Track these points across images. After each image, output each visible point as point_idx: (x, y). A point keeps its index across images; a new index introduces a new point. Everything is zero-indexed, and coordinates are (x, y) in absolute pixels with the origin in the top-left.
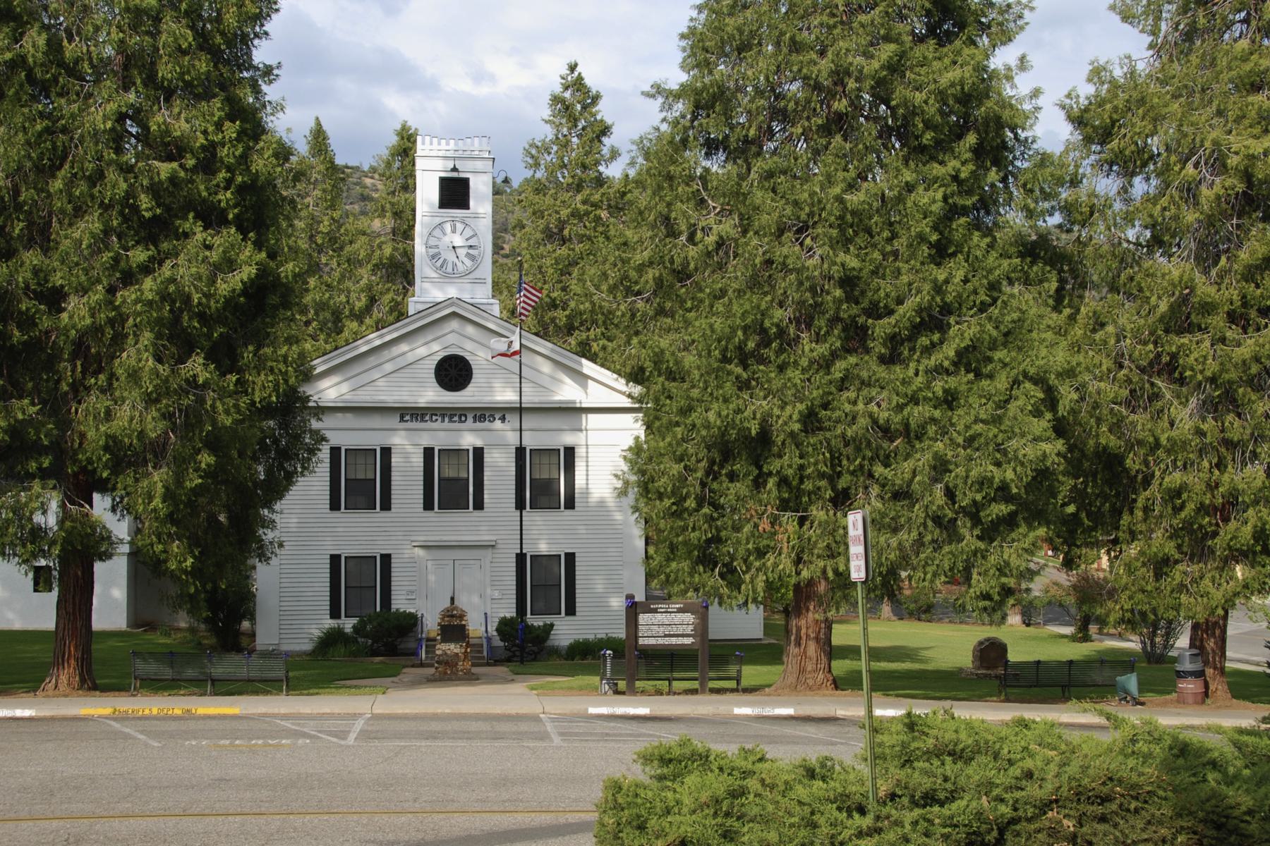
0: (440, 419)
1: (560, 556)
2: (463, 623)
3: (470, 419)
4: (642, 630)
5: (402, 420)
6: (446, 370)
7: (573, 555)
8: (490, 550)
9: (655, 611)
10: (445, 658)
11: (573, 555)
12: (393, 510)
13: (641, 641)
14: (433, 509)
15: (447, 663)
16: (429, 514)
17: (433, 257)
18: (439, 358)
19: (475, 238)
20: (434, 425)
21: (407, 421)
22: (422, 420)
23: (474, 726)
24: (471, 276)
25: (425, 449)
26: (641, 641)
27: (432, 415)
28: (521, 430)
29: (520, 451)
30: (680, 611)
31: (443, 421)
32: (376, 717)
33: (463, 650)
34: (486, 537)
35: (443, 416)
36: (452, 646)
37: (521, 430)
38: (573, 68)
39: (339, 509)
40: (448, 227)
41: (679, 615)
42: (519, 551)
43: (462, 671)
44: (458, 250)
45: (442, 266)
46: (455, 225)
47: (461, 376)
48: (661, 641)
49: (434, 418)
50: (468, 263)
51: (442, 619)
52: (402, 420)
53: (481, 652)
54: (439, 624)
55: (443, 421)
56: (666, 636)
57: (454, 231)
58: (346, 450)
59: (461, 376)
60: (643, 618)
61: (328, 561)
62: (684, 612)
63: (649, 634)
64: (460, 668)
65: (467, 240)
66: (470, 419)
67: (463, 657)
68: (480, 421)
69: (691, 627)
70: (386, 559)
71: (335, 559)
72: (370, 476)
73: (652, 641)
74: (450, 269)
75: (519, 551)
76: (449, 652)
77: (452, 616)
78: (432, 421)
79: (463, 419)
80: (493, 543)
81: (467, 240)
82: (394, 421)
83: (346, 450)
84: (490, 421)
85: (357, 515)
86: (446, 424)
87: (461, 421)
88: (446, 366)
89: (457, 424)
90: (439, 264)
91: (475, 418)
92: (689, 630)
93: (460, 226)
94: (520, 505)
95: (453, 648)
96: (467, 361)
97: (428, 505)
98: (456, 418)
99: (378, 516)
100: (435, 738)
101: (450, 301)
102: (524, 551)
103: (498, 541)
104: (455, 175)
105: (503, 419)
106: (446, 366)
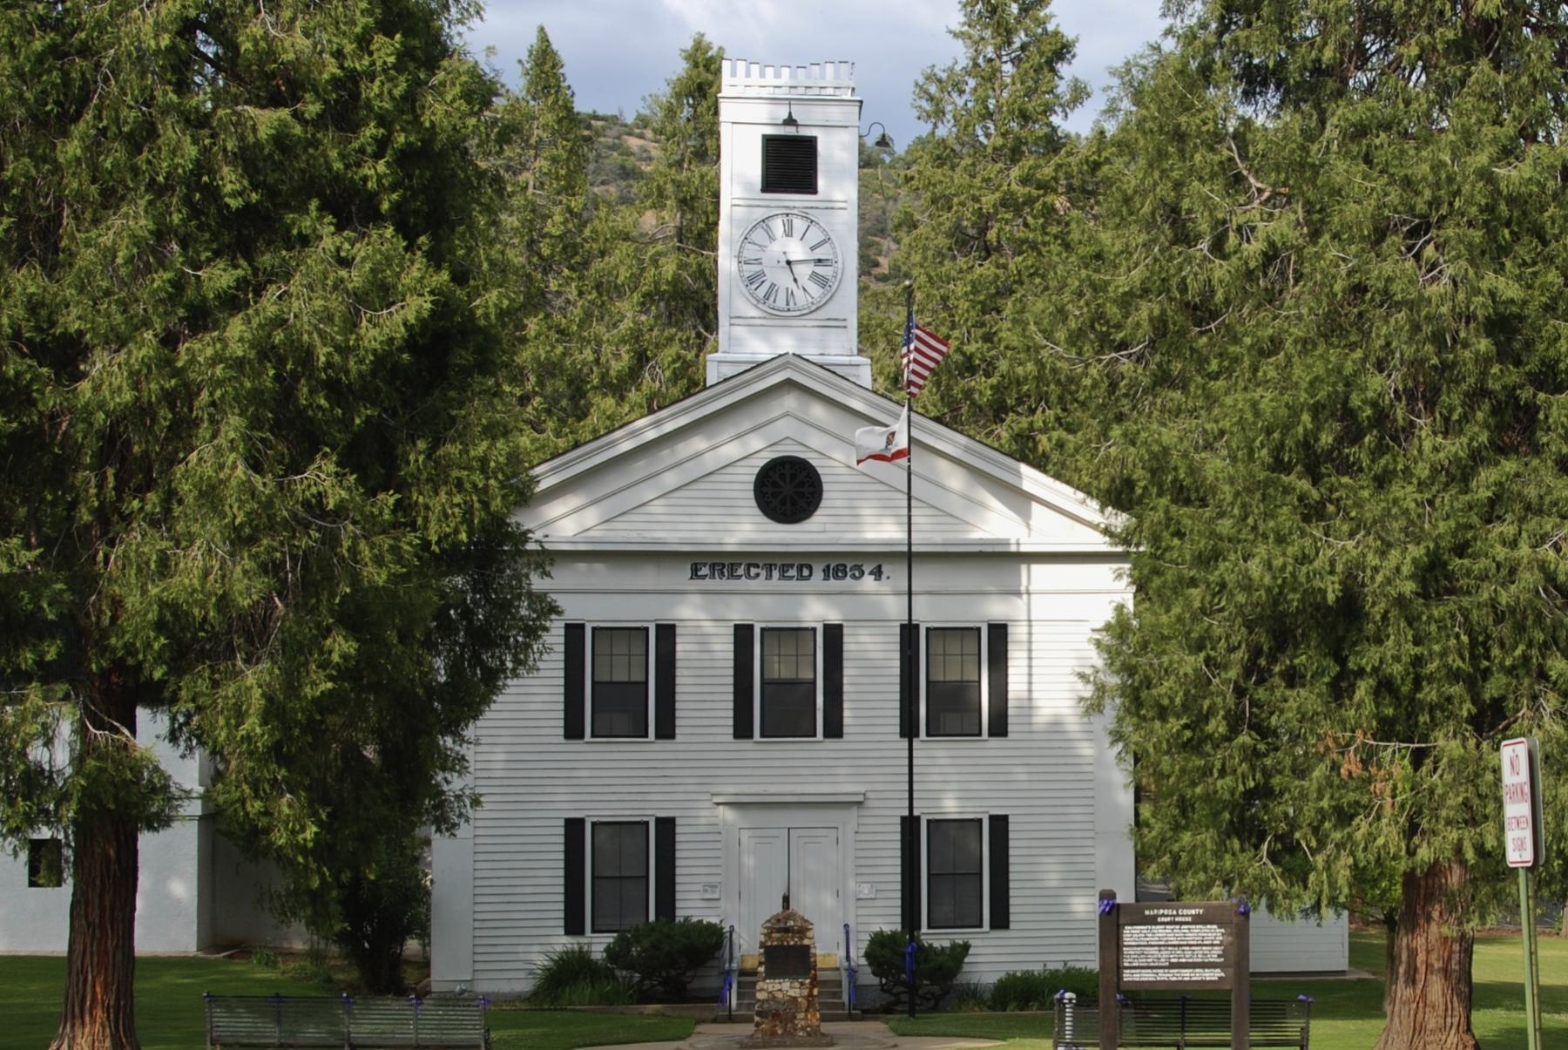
0: (763, 573)
1: (647, 823)
2: (806, 942)
3: (818, 574)
4: (1129, 956)
5: (695, 574)
8: (854, 811)
9: (1153, 921)
10: (774, 1006)
11: (1005, 818)
13: (1128, 976)
16: (744, 744)
17: (751, 280)
18: (762, 463)
21: (704, 577)
22: (732, 576)
25: (737, 627)
26: (1128, 976)
27: (749, 566)
29: (909, 632)
30: (1197, 920)
31: (769, 577)
33: (806, 992)
34: (847, 787)
36: (786, 985)
40: (778, 226)
41: (1197, 929)
42: (906, 813)
43: (803, 1028)
44: (795, 267)
45: (767, 297)
46: (791, 224)
48: (1163, 975)
49: (753, 571)
50: (815, 290)
51: (768, 935)
52: (695, 574)
53: (838, 995)
54: (762, 945)
56: (1172, 966)
57: (789, 233)
58: (594, 629)
60: (1132, 934)
61: (562, 831)
63: (1143, 962)
64: (800, 1023)
65: (813, 249)
66: (818, 574)
68: (836, 577)
69: (1218, 950)
71: (574, 828)
72: (637, 676)
73: (1147, 976)
74: (781, 303)
75: (906, 813)
76: (780, 995)
77: (786, 930)
78: (748, 576)
79: (806, 572)
80: (861, 798)
81: (813, 249)
82: (679, 577)
83: (594, 629)
84: (854, 577)
86: (776, 582)
87: (801, 577)
89: (794, 582)
91: (826, 571)
92: (1214, 955)
93: (798, 224)
94: (909, 729)
97: (742, 729)
98: (793, 572)
99: (651, 750)
102: (916, 813)
103: (869, 795)
104: (790, 131)
105: (878, 573)
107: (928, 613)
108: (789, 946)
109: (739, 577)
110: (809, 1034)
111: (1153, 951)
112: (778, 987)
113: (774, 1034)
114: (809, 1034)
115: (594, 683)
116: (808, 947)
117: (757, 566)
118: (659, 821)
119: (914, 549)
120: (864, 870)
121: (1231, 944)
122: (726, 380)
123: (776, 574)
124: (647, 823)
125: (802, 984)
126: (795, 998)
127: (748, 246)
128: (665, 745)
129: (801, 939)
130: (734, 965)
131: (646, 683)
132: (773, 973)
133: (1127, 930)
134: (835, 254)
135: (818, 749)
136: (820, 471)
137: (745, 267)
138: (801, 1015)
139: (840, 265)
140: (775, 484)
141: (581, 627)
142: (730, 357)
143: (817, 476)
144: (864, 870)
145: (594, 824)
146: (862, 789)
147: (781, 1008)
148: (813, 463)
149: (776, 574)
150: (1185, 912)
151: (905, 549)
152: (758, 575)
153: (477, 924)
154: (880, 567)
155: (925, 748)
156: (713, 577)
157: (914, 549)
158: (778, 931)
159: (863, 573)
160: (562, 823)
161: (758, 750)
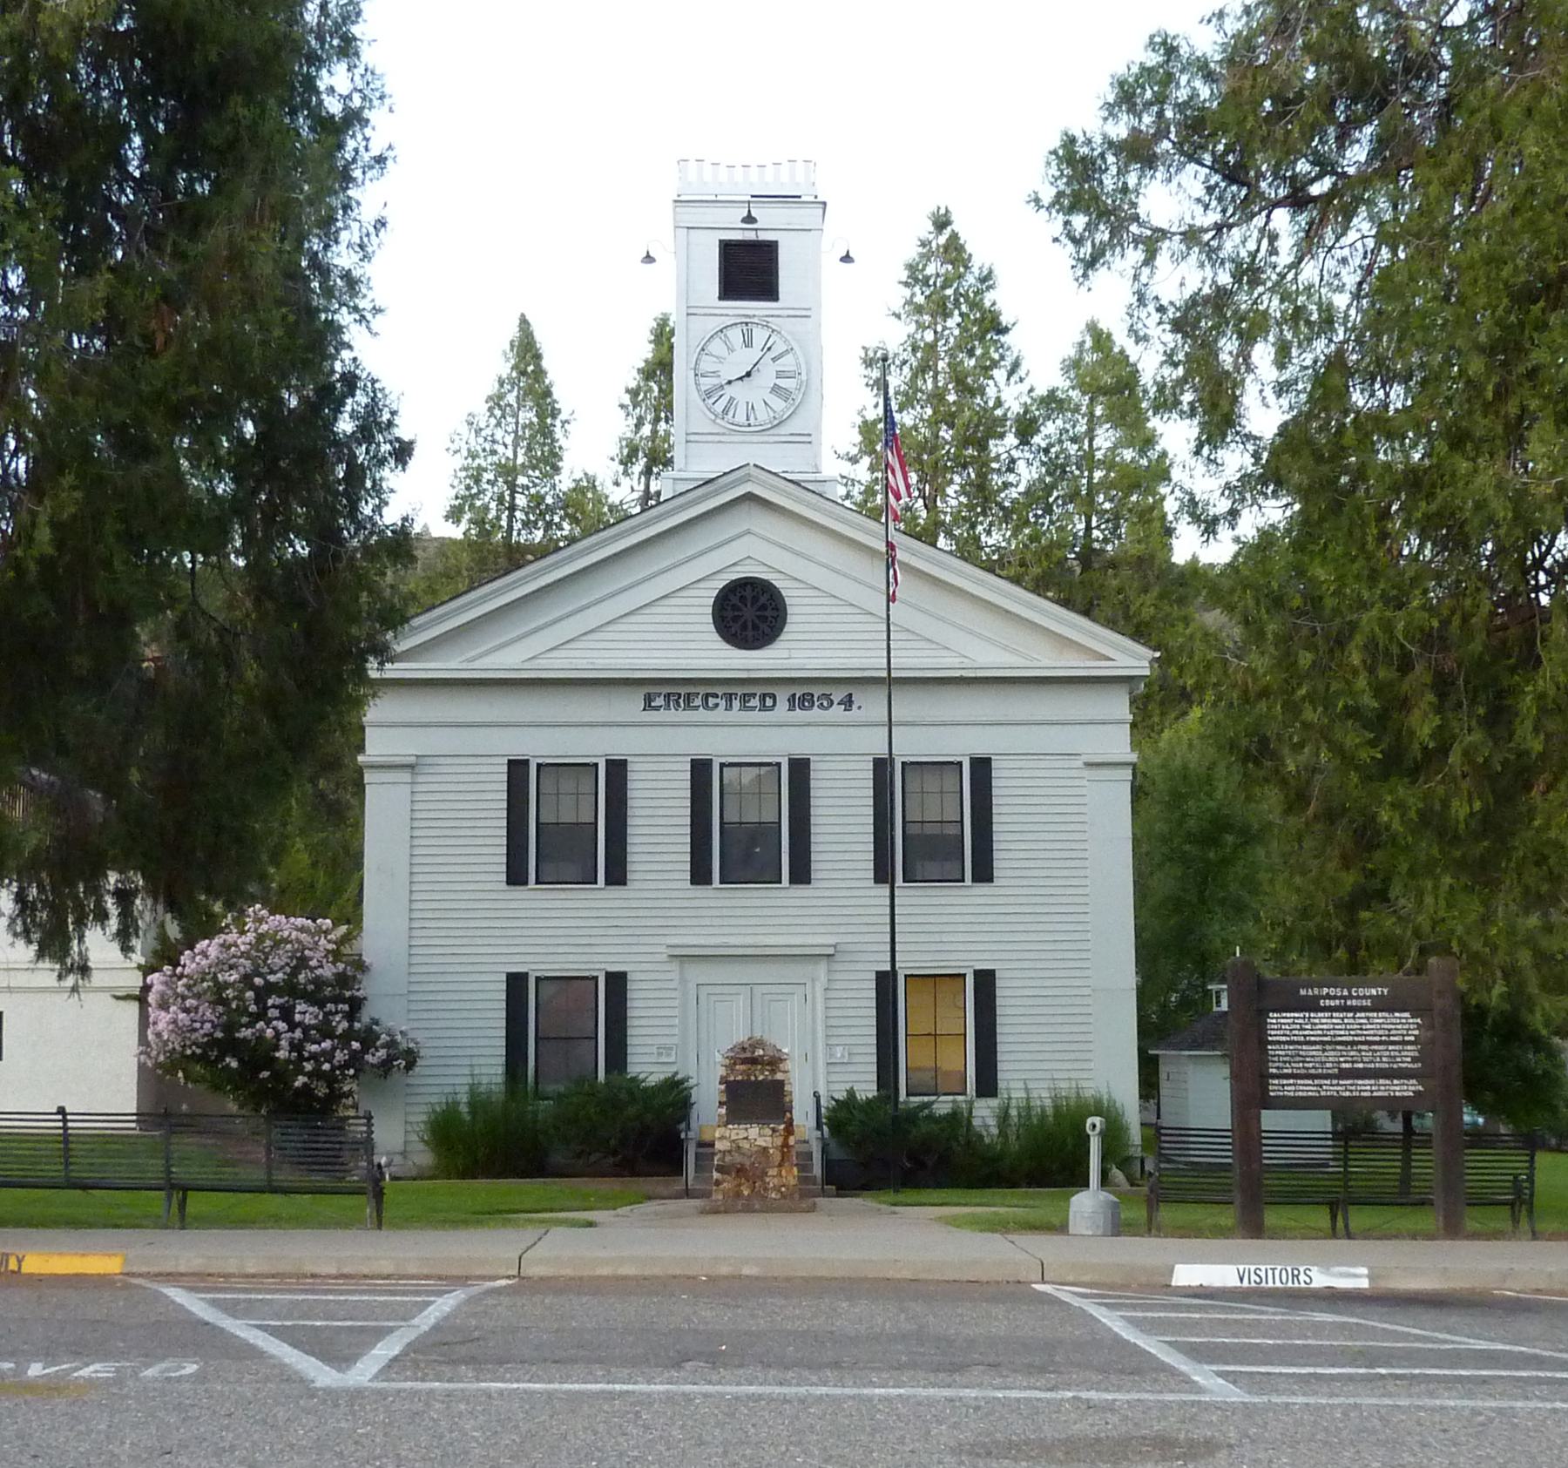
0: (723, 703)
1: (596, 978)
2: (779, 1076)
3: (782, 704)
5: (648, 704)
6: (735, 619)
8: (821, 969)
9: (1312, 1005)
10: (738, 1159)
12: (996, 882)
14: (710, 883)
15: (740, 1171)
16: (701, 891)
17: (709, 394)
18: (722, 584)
19: (789, 357)
20: (711, 716)
21: (657, 708)
22: (689, 706)
23: (852, 1316)
24: (783, 430)
29: (882, 768)
30: (1379, 1005)
31: (729, 707)
32: (526, 1285)
33: (779, 1141)
34: (822, 940)
35: (729, 698)
36: (754, 1131)
38: (941, 223)
39: (709, 882)
40: (736, 336)
41: (1379, 1018)
43: (777, 1189)
45: (725, 411)
47: (763, 607)
49: (712, 701)
50: (778, 404)
51: (730, 1068)
54: (723, 1080)
55: (729, 707)
56: (1343, 1074)
58: (539, 766)
59: (763, 607)
62: (1391, 1010)
64: (772, 1182)
66: (782, 704)
67: (777, 1157)
69: (1411, 1051)
70: (617, 981)
71: (516, 983)
72: (587, 817)
74: (741, 418)
76: (745, 1145)
77: (754, 1061)
78: (706, 707)
79: (769, 702)
80: (831, 951)
82: (630, 706)
85: (563, 895)
86: (736, 714)
87: (764, 708)
88: (735, 600)
90: (719, 407)
92: (1407, 1058)
93: (759, 336)
94: (883, 874)
95: (756, 1136)
97: (700, 875)
98: (755, 702)
99: (600, 897)
100: (714, 1360)
101: (738, 473)
104: (751, 236)
105: (848, 702)
106: (735, 600)
107: (911, 746)
110: (784, 1196)
111: (1314, 1051)
112: (743, 1134)
113: (738, 1195)
114: (784, 1196)
115: (722, 823)
116: (781, 1083)
119: (893, 675)
121: (1432, 1041)
122: (680, 494)
123: (736, 704)
125: (774, 1130)
126: (765, 1149)
127: (704, 357)
128: (616, 892)
129: (773, 1072)
130: (691, 1135)
133: (1273, 1018)
134: (798, 365)
135: (783, 897)
136: (784, 593)
137: (702, 380)
139: (804, 377)
140: (735, 608)
141: (525, 763)
142: (684, 475)
145: (538, 979)
146: (832, 940)
147: (747, 1163)
149: (736, 704)
150: (1361, 991)
151: (884, 674)
152: (717, 705)
154: (850, 695)
155: (911, 897)
156: (668, 707)
157: (893, 675)
158: (744, 1061)
160: (504, 978)
161: (717, 896)
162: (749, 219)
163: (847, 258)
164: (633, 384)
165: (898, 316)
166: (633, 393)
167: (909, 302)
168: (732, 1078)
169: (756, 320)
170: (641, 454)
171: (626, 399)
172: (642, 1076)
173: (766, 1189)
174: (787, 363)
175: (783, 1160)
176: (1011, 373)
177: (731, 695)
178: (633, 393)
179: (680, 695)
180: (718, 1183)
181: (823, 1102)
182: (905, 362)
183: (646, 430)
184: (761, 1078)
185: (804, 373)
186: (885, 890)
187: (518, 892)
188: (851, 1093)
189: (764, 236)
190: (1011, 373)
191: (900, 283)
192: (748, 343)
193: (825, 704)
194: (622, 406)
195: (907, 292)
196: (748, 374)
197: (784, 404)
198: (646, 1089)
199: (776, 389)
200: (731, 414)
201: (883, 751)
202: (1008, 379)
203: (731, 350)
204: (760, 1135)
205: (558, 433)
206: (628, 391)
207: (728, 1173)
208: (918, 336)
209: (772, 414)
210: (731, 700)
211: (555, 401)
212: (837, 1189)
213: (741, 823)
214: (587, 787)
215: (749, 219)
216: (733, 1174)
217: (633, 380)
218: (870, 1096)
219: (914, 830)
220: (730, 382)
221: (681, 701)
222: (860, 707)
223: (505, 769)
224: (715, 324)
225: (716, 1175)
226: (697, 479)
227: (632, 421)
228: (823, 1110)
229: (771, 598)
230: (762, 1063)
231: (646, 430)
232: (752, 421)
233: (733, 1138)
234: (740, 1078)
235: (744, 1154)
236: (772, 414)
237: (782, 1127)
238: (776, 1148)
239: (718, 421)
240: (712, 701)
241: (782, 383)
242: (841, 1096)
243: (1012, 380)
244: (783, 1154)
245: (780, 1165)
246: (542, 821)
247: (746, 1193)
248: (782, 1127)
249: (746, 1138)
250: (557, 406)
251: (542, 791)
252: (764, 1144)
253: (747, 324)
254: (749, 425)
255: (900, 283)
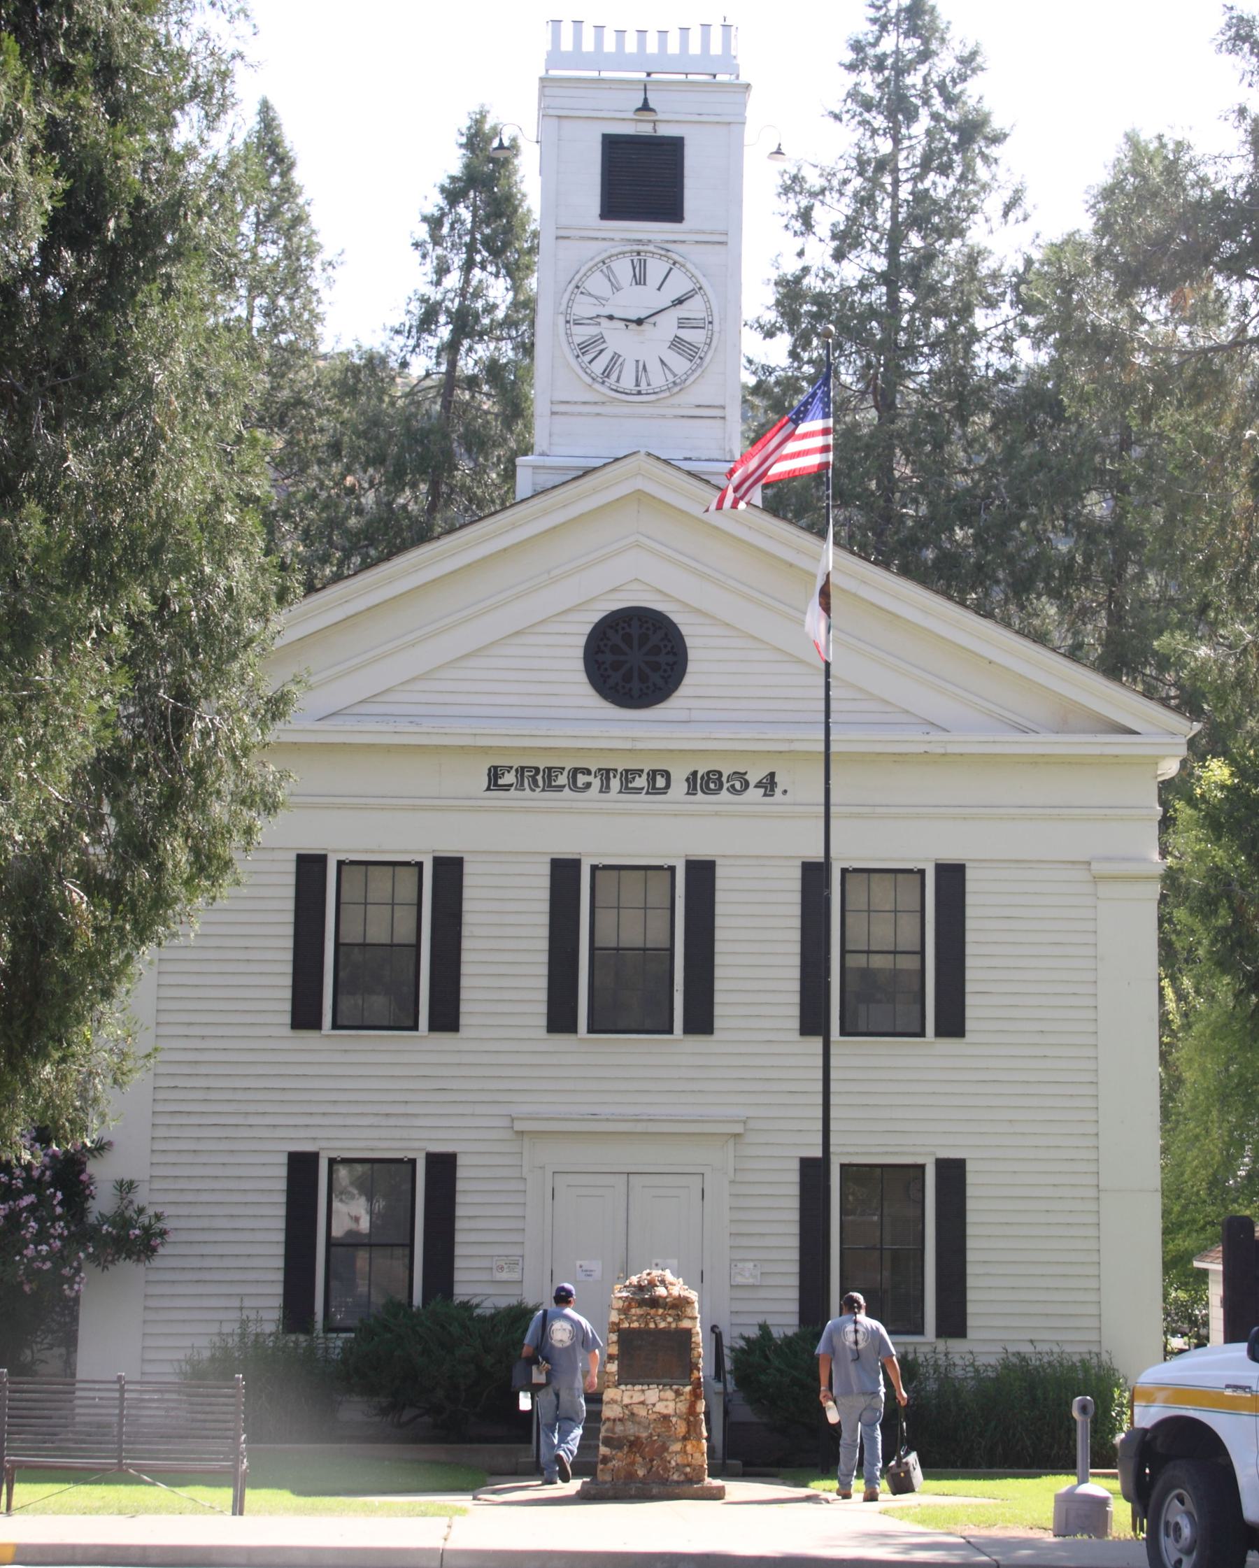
0: (596, 783)
1: (413, 1162)
7: (234, 1514)
10: (631, 1430)
11: (234, 1514)
15: (634, 1444)
16: (562, 1041)
17: (583, 348)
21: (507, 787)
22: (1206, 1324)
25: (804, 864)
28: (895, 953)
33: (683, 1407)
36: (652, 1394)
37: (895, 953)
39: (572, 1028)
40: (623, 269)
45: (607, 373)
49: (582, 779)
50: (680, 364)
67: (681, 1428)
74: (628, 382)
76: (642, 1412)
77: (655, 1302)
79: (661, 782)
80: (738, 1129)
84: (732, 790)
89: (643, 796)
90: (599, 366)
93: (656, 269)
96: (673, 626)
104: (645, 129)
108: (663, 1331)
109: (560, 788)
112: (638, 1397)
115: (338, 945)
117: (588, 772)
118: (432, 1159)
120: (744, 1242)
123: (615, 784)
124: (413, 1162)
126: (666, 1418)
129: (678, 1318)
131: (417, 946)
132: (628, 1376)
134: (709, 309)
138: (677, 1447)
139: (716, 327)
142: (548, 461)
143: (680, 637)
144: (744, 1242)
148: (676, 618)
152: (588, 785)
153: (157, 1158)
156: (520, 787)
158: (643, 1302)
159: (746, 785)
162: (645, 107)
163: (779, 152)
164: (432, 210)
165: (837, 117)
166: (434, 223)
167: (854, 94)
168: (626, 1325)
169: (651, 248)
170: (443, 319)
171: (423, 232)
172: (475, 1301)
173: (666, 1469)
174: (694, 308)
175: (688, 1432)
176: (1008, 209)
177: (608, 771)
178: (434, 223)
179: (537, 770)
180: (605, 1460)
181: (726, 1341)
182: (845, 182)
183: (453, 280)
184: (662, 1325)
185: (716, 322)
186: (816, 1043)
187: (308, 1038)
188: (764, 1328)
189: (665, 131)
190: (1008, 209)
191: (841, 65)
192: (640, 279)
193: (738, 786)
194: (416, 245)
195: (851, 79)
196: (639, 322)
197: (688, 364)
198: (482, 1319)
199: (677, 344)
200: (614, 376)
201: (817, 854)
202: (1005, 215)
203: (616, 288)
204: (661, 1400)
205: (316, 281)
206: (425, 219)
207: (620, 1448)
208: (869, 145)
209: (671, 378)
210: (608, 779)
211: (313, 232)
212: (746, 1464)
213: (645, 949)
214: (657, 895)
215: (645, 107)
216: (626, 1449)
217: (434, 202)
218: (790, 1332)
219: (855, 961)
220: (611, 318)
221: (539, 778)
222: (785, 792)
223: (292, 867)
224: (592, 250)
225: (603, 1450)
226: (568, 468)
227: (430, 266)
228: (726, 1351)
229: (672, 665)
230: (665, 1306)
231: (453, 280)
232: (643, 386)
233: (626, 1401)
234: (635, 1325)
235: (639, 1423)
236: (671, 378)
237: (688, 1388)
238: (680, 1417)
239: (597, 386)
240: (582, 779)
241: (686, 335)
242: (754, 1333)
243: (1012, 216)
244: (688, 1423)
245: (685, 1438)
246: (597, 945)
247: (641, 1473)
248: (688, 1388)
249: (642, 1403)
250: (315, 239)
251: (344, 899)
252: (665, 1411)
253: (639, 253)
254: (639, 393)
255: (841, 65)
